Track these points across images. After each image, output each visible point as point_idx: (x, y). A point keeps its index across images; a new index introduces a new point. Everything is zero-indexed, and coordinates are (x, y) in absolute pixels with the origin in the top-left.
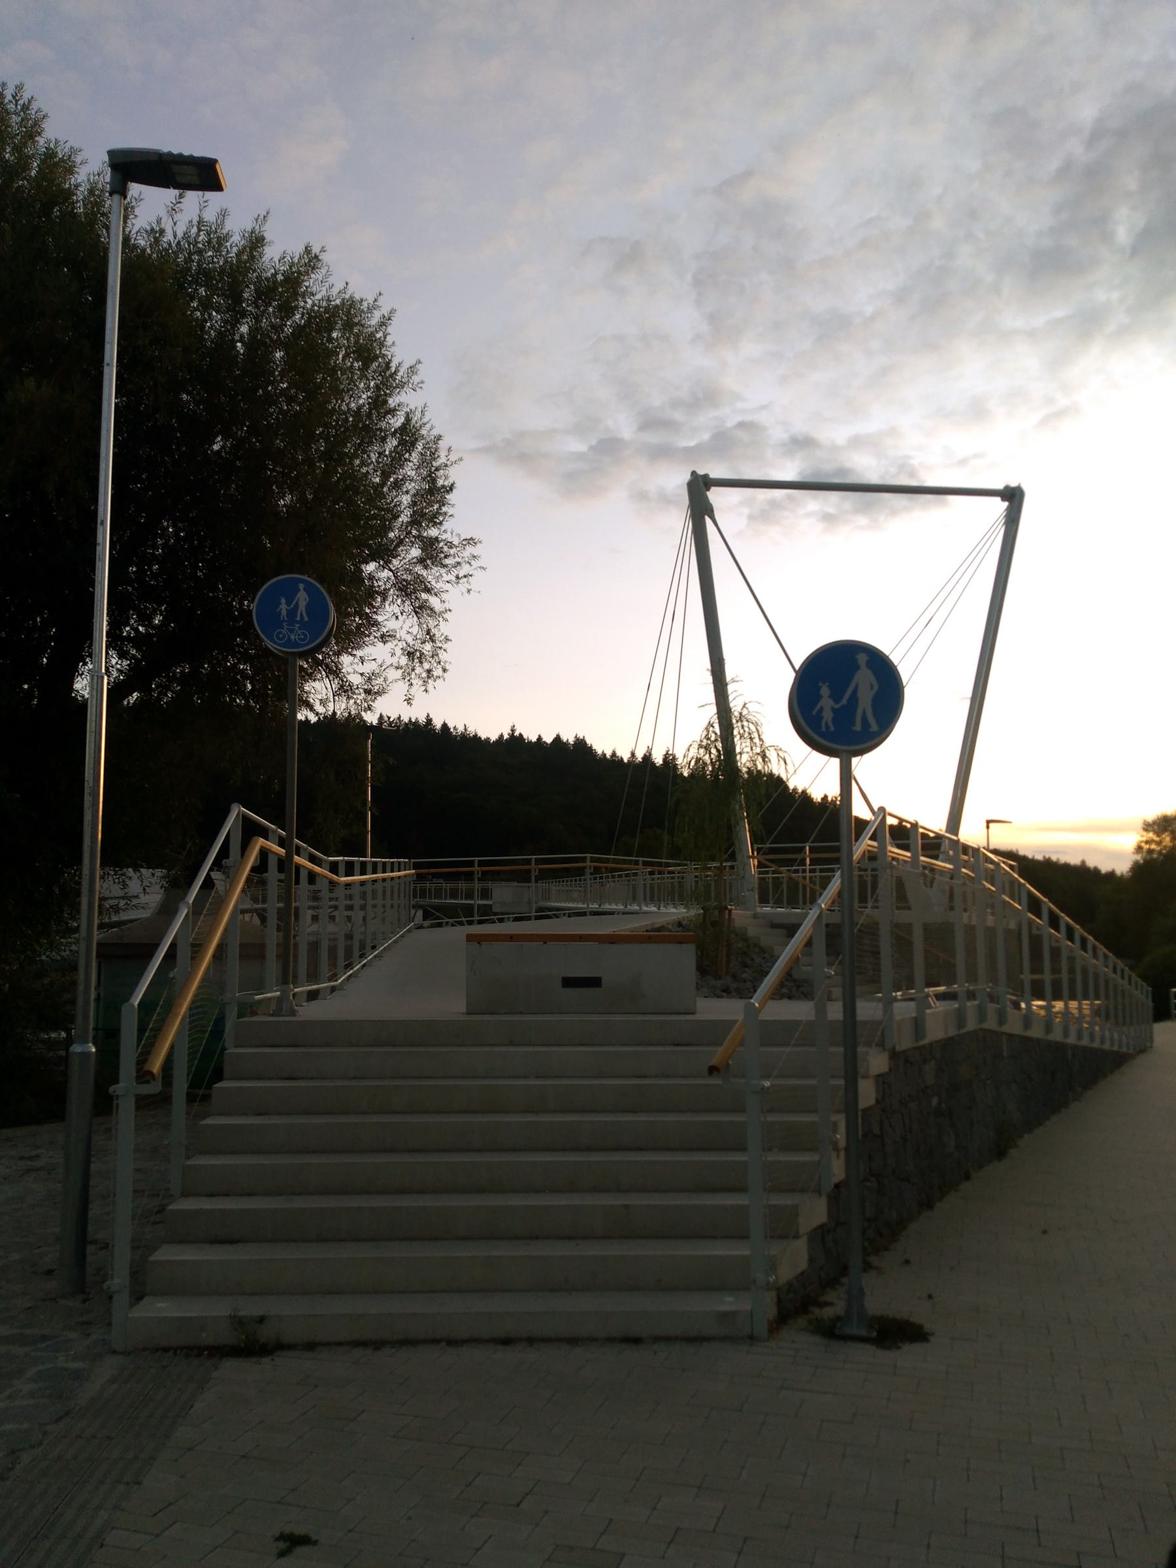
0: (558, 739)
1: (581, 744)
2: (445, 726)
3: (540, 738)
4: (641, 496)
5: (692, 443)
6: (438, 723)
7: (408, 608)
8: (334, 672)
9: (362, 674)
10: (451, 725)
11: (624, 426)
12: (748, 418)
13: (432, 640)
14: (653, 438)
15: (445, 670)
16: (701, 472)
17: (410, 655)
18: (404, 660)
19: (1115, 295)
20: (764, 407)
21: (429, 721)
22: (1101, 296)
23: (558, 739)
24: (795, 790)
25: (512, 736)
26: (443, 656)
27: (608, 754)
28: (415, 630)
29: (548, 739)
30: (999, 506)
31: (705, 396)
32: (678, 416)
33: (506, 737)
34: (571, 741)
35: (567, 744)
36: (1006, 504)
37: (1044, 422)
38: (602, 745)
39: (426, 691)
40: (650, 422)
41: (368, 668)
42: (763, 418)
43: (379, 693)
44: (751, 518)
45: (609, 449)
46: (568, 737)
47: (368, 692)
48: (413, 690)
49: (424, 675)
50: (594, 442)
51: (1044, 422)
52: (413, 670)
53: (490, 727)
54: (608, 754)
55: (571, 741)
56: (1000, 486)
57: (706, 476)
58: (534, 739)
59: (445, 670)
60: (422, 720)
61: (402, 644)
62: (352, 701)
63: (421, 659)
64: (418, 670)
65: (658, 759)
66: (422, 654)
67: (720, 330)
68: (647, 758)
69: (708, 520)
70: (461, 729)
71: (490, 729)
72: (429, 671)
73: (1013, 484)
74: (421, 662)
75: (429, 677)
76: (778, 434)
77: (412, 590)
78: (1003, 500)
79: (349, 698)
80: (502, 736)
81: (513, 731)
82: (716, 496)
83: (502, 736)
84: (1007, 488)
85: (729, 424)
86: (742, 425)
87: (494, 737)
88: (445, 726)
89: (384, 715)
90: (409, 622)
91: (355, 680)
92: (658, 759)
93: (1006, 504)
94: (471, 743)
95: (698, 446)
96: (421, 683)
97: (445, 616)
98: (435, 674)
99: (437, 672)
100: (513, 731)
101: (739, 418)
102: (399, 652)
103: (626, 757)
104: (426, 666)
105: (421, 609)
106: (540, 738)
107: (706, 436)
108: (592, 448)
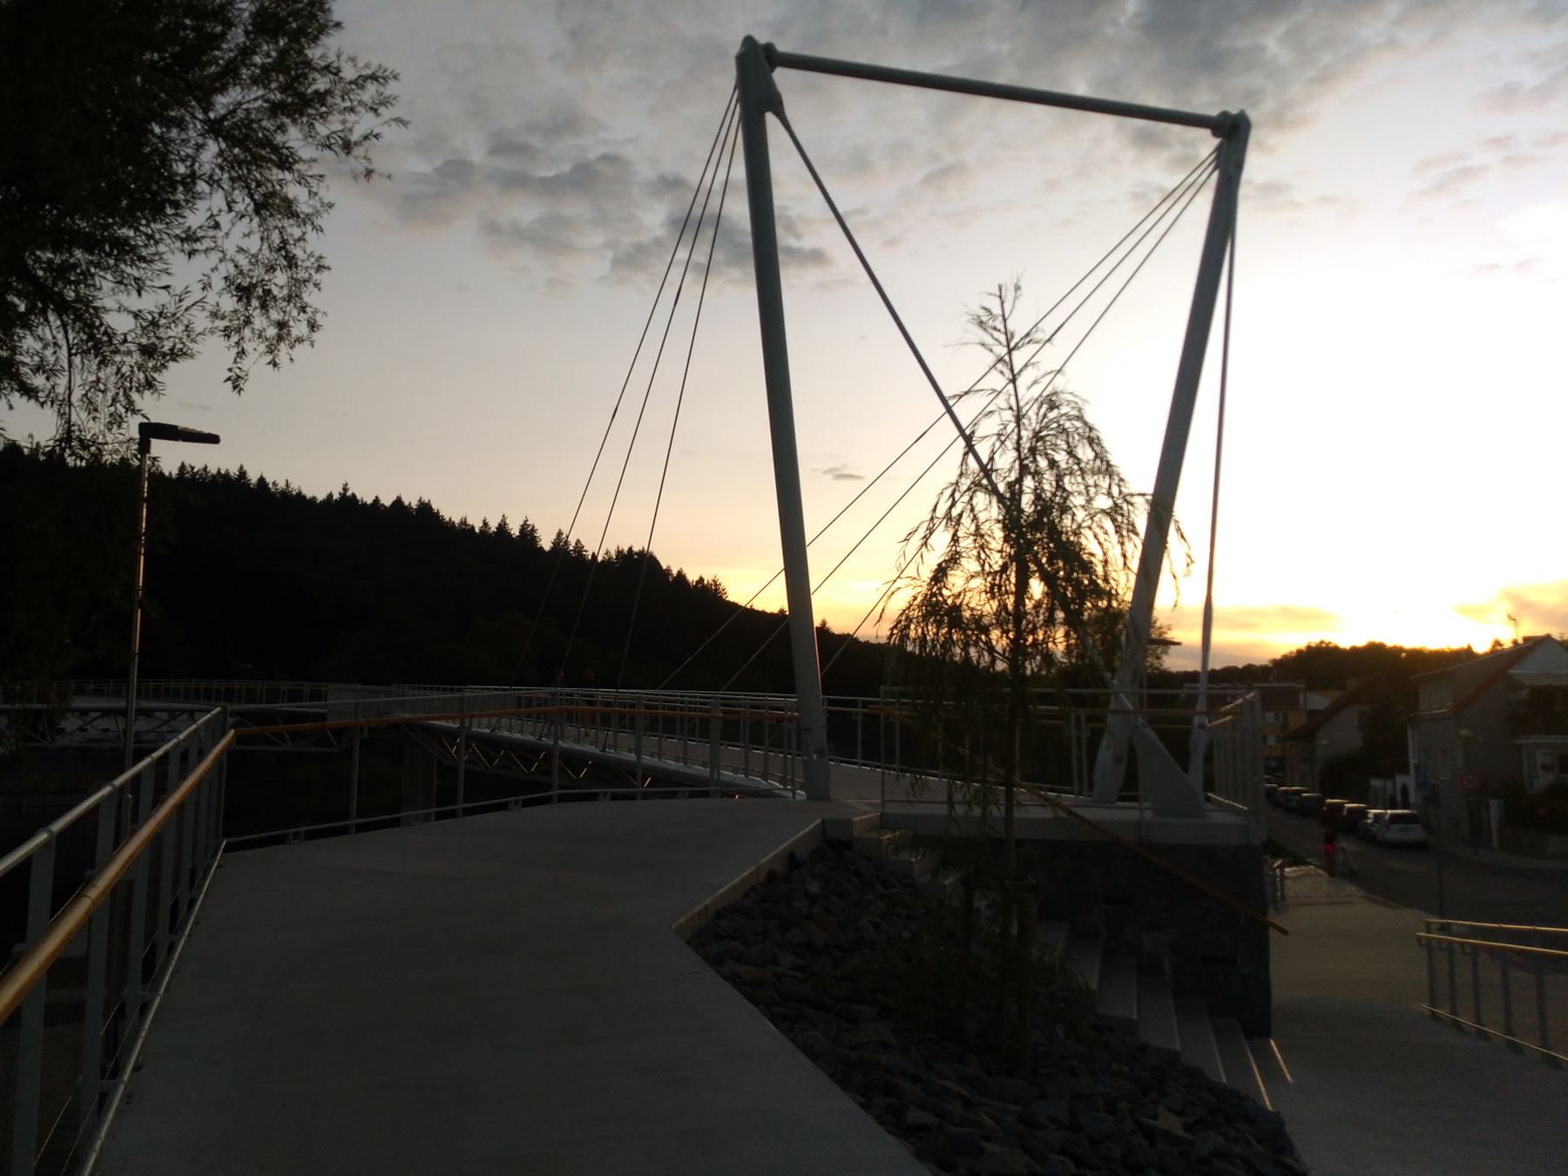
0: (398, 502)
1: (425, 508)
2: (262, 480)
3: (377, 500)
4: (492, 228)
5: (550, 174)
6: (253, 477)
7: (243, 203)
8: (83, 316)
9: (136, 315)
10: (269, 480)
11: (477, 153)
12: (611, 150)
13: (291, 262)
14: (507, 164)
15: (313, 326)
16: (762, 39)
17: (244, 292)
18: (229, 303)
19: (1006, 47)
20: (631, 140)
21: (242, 474)
22: (991, 46)
23: (398, 502)
24: (668, 571)
25: (343, 495)
26: (310, 296)
27: (457, 520)
28: (253, 244)
29: (387, 501)
30: (1206, 144)
31: (566, 122)
32: (535, 141)
33: (336, 496)
34: (414, 505)
35: (409, 508)
36: (1216, 141)
37: (929, 180)
38: (451, 512)
39: (275, 365)
40: (503, 146)
41: (149, 302)
42: (629, 152)
43: (175, 355)
44: (616, 262)
45: (456, 172)
46: (411, 500)
47: (148, 351)
48: (246, 363)
49: (272, 332)
50: (438, 163)
51: (929, 180)
52: (248, 322)
53: (317, 482)
54: (457, 520)
55: (414, 505)
56: (1214, 112)
57: (769, 48)
58: (369, 501)
59: (313, 326)
60: (234, 471)
61: (227, 269)
62: (111, 370)
63: (269, 303)
64: (259, 321)
65: (515, 531)
66: (268, 292)
67: (583, 47)
68: (502, 527)
69: (771, 119)
70: (282, 485)
71: (318, 485)
72: (282, 325)
73: (1234, 111)
74: (264, 306)
75: (280, 338)
76: (646, 172)
77: (253, 154)
78: (1215, 134)
79: (103, 363)
80: (330, 495)
81: (345, 490)
82: (783, 78)
83: (330, 495)
84: (1224, 115)
85: (592, 155)
86: (607, 158)
87: (837, 632)
88: (262, 480)
89: (187, 463)
90: (243, 226)
91: (120, 323)
92: (515, 531)
93: (1216, 141)
94: (293, 503)
95: (557, 177)
96: (262, 348)
97: (318, 222)
98: (295, 332)
99: (299, 328)
100: (345, 490)
101: (602, 150)
102: (218, 283)
103: (478, 526)
104: (275, 315)
105: (270, 205)
106: (377, 500)
107: (566, 168)
108: (437, 170)
